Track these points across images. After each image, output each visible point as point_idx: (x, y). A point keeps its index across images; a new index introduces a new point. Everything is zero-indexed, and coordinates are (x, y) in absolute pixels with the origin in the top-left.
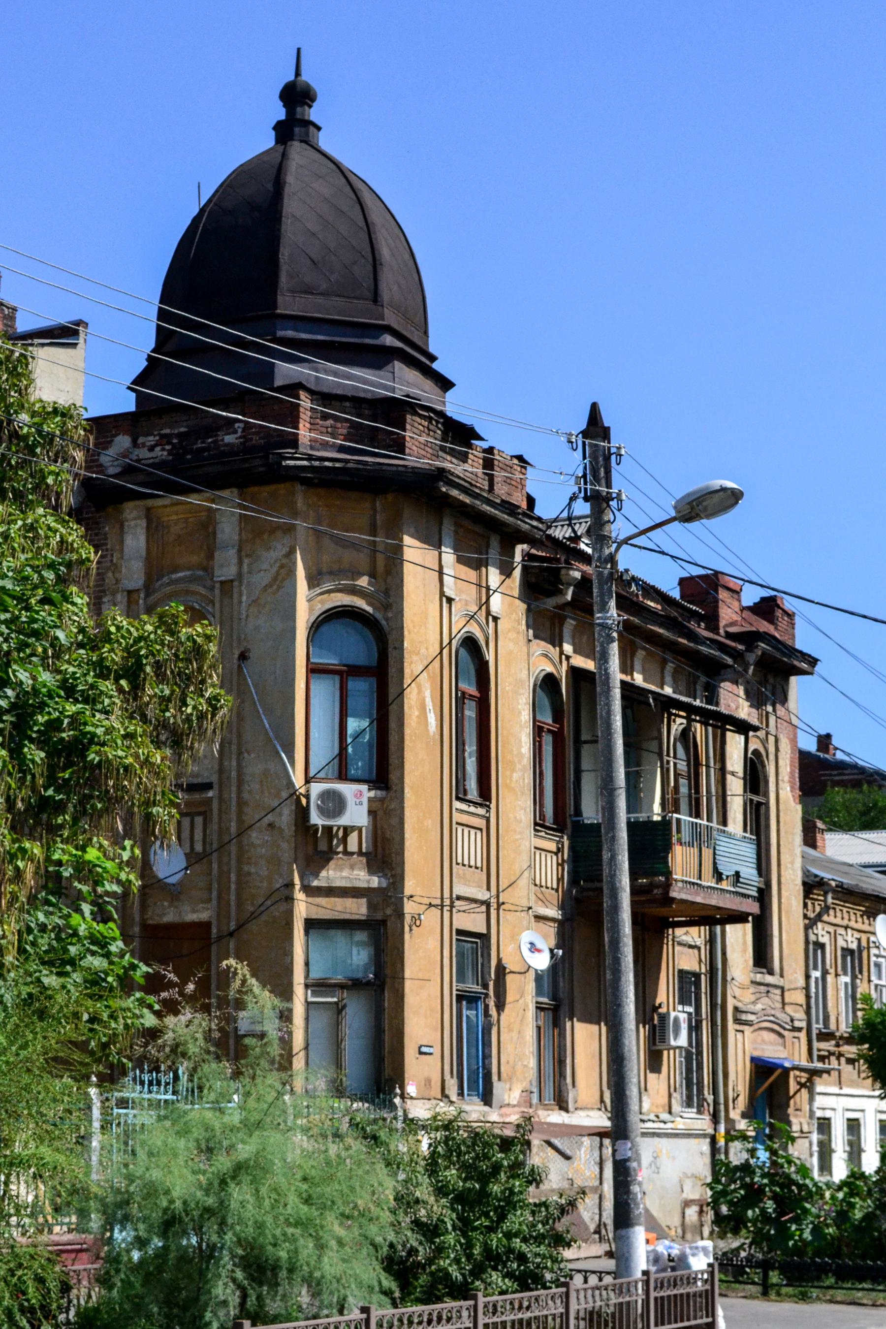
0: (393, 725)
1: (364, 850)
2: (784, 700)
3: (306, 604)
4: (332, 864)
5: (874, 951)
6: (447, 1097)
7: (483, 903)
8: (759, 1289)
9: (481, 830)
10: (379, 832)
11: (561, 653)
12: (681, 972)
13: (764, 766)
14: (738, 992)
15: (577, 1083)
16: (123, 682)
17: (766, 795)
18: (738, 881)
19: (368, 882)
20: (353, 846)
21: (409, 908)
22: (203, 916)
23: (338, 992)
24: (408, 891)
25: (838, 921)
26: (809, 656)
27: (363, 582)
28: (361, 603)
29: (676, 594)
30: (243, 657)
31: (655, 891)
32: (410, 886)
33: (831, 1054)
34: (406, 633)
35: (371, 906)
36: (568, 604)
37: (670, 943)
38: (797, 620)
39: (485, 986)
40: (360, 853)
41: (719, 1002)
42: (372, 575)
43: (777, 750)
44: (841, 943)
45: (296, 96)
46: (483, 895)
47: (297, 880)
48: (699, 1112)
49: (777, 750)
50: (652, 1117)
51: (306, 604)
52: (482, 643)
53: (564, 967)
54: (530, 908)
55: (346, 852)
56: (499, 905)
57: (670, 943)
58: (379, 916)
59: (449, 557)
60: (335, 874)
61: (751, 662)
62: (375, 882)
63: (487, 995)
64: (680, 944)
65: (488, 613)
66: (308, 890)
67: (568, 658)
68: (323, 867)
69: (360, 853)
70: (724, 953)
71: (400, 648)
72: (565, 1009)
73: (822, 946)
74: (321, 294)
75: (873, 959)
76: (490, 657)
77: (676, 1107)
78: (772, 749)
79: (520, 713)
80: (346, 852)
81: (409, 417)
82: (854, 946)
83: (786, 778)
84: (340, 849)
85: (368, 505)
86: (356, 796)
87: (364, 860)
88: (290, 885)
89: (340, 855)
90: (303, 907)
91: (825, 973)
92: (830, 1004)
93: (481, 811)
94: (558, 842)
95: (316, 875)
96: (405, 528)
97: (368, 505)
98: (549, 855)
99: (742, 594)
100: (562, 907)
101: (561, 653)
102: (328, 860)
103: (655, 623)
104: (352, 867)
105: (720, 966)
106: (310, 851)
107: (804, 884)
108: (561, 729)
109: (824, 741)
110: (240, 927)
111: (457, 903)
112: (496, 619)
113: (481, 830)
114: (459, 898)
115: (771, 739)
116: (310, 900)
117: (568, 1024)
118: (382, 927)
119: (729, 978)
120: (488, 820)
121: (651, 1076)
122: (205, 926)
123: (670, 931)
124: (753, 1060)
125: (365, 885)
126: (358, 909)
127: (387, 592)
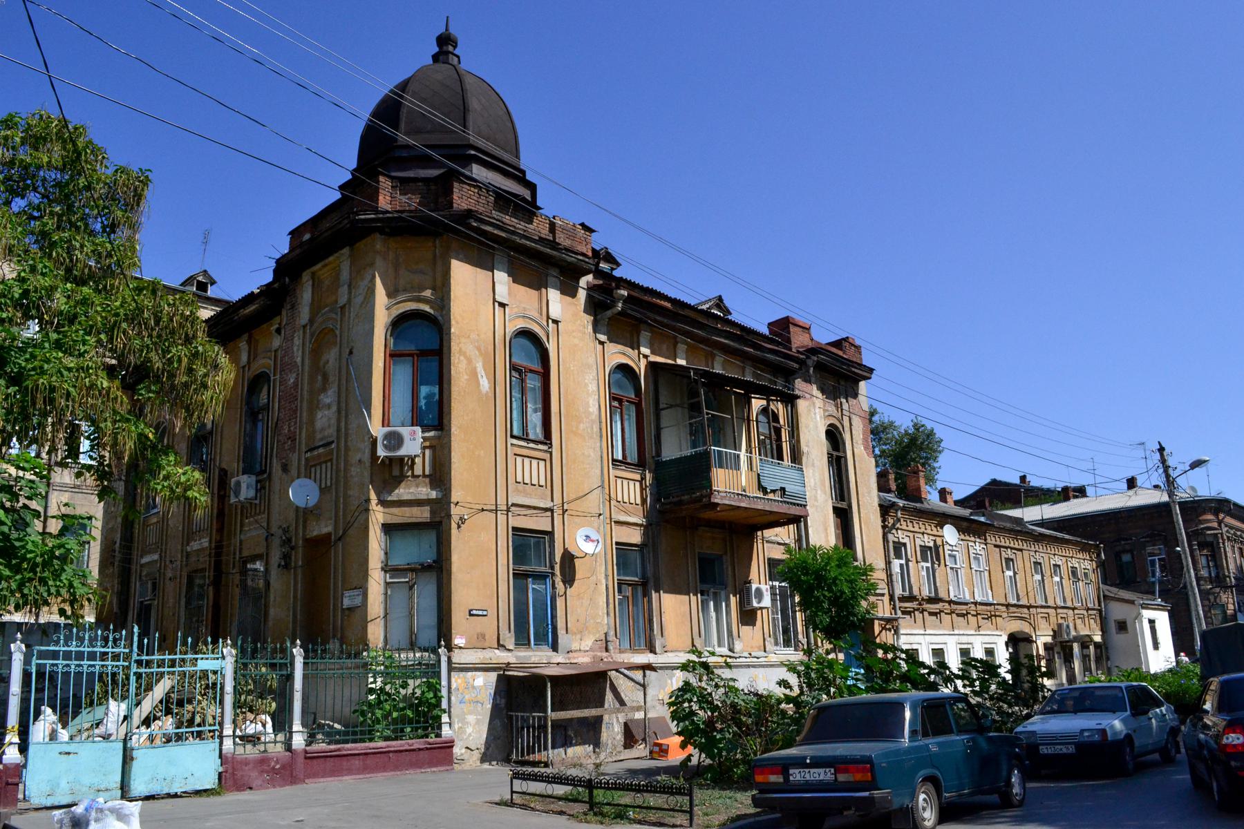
1: (427, 472)
2: (855, 395)
3: (383, 310)
4: (403, 485)
5: (947, 547)
6: (503, 646)
7: (546, 510)
8: (585, 807)
15: (665, 633)
16: (103, 336)
17: (845, 452)
20: (418, 470)
21: (455, 511)
22: (325, 530)
23: (409, 575)
24: (454, 499)
25: (916, 529)
27: (428, 293)
28: (427, 308)
29: (765, 331)
30: (351, 353)
32: (455, 496)
33: (915, 610)
34: (453, 322)
35: (432, 512)
36: (620, 313)
37: (760, 546)
38: (863, 350)
39: (552, 568)
40: (424, 476)
42: (434, 289)
44: (919, 542)
45: (445, 41)
46: (549, 505)
47: (373, 496)
48: (796, 650)
50: (746, 654)
51: (383, 310)
52: (545, 339)
55: (413, 476)
56: (564, 511)
57: (760, 546)
58: (438, 519)
59: (501, 277)
60: (404, 492)
62: (434, 494)
63: (553, 574)
65: (548, 317)
66: (382, 503)
67: (646, 357)
68: (396, 488)
69: (424, 476)
71: (449, 334)
72: (651, 583)
73: (905, 545)
74: (428, 132)
75: (947, 553)
76: (551, 348)
77: (769, 647)
78: (846, 424)
79: (586, 385)
80: (413, 476)
81: (456, 185)
82: (931, 544)
83: (860, 442)
84: (410, 473)
85: (430, 244)
87: (427, 480)
88: (368, 501)
90: (378, 516)
91: (908, 561)
92: (912, 580)
93: (545, 448)
95: (390, 492)
97: (430, 244)
98: (631, 483)
99: (812, 331)
100: (647, 516)
102: (400, 483)
103: (718, 336)
104: (417, 486)
106: (387, 476)
107: (880, 506)
108: (640, 401)
109: (1023, 478)
110: (344, 533)
111: (513, 509)
112: (556, 322)
114: (513, 505)
115: (846, 419)
116: (387, 510)
117: (654, 595)
118: (437, 525)
120: (551, 453)
121: (746, 629)
122: (329, 534)
126: (423, 514)
127: (442, 300)
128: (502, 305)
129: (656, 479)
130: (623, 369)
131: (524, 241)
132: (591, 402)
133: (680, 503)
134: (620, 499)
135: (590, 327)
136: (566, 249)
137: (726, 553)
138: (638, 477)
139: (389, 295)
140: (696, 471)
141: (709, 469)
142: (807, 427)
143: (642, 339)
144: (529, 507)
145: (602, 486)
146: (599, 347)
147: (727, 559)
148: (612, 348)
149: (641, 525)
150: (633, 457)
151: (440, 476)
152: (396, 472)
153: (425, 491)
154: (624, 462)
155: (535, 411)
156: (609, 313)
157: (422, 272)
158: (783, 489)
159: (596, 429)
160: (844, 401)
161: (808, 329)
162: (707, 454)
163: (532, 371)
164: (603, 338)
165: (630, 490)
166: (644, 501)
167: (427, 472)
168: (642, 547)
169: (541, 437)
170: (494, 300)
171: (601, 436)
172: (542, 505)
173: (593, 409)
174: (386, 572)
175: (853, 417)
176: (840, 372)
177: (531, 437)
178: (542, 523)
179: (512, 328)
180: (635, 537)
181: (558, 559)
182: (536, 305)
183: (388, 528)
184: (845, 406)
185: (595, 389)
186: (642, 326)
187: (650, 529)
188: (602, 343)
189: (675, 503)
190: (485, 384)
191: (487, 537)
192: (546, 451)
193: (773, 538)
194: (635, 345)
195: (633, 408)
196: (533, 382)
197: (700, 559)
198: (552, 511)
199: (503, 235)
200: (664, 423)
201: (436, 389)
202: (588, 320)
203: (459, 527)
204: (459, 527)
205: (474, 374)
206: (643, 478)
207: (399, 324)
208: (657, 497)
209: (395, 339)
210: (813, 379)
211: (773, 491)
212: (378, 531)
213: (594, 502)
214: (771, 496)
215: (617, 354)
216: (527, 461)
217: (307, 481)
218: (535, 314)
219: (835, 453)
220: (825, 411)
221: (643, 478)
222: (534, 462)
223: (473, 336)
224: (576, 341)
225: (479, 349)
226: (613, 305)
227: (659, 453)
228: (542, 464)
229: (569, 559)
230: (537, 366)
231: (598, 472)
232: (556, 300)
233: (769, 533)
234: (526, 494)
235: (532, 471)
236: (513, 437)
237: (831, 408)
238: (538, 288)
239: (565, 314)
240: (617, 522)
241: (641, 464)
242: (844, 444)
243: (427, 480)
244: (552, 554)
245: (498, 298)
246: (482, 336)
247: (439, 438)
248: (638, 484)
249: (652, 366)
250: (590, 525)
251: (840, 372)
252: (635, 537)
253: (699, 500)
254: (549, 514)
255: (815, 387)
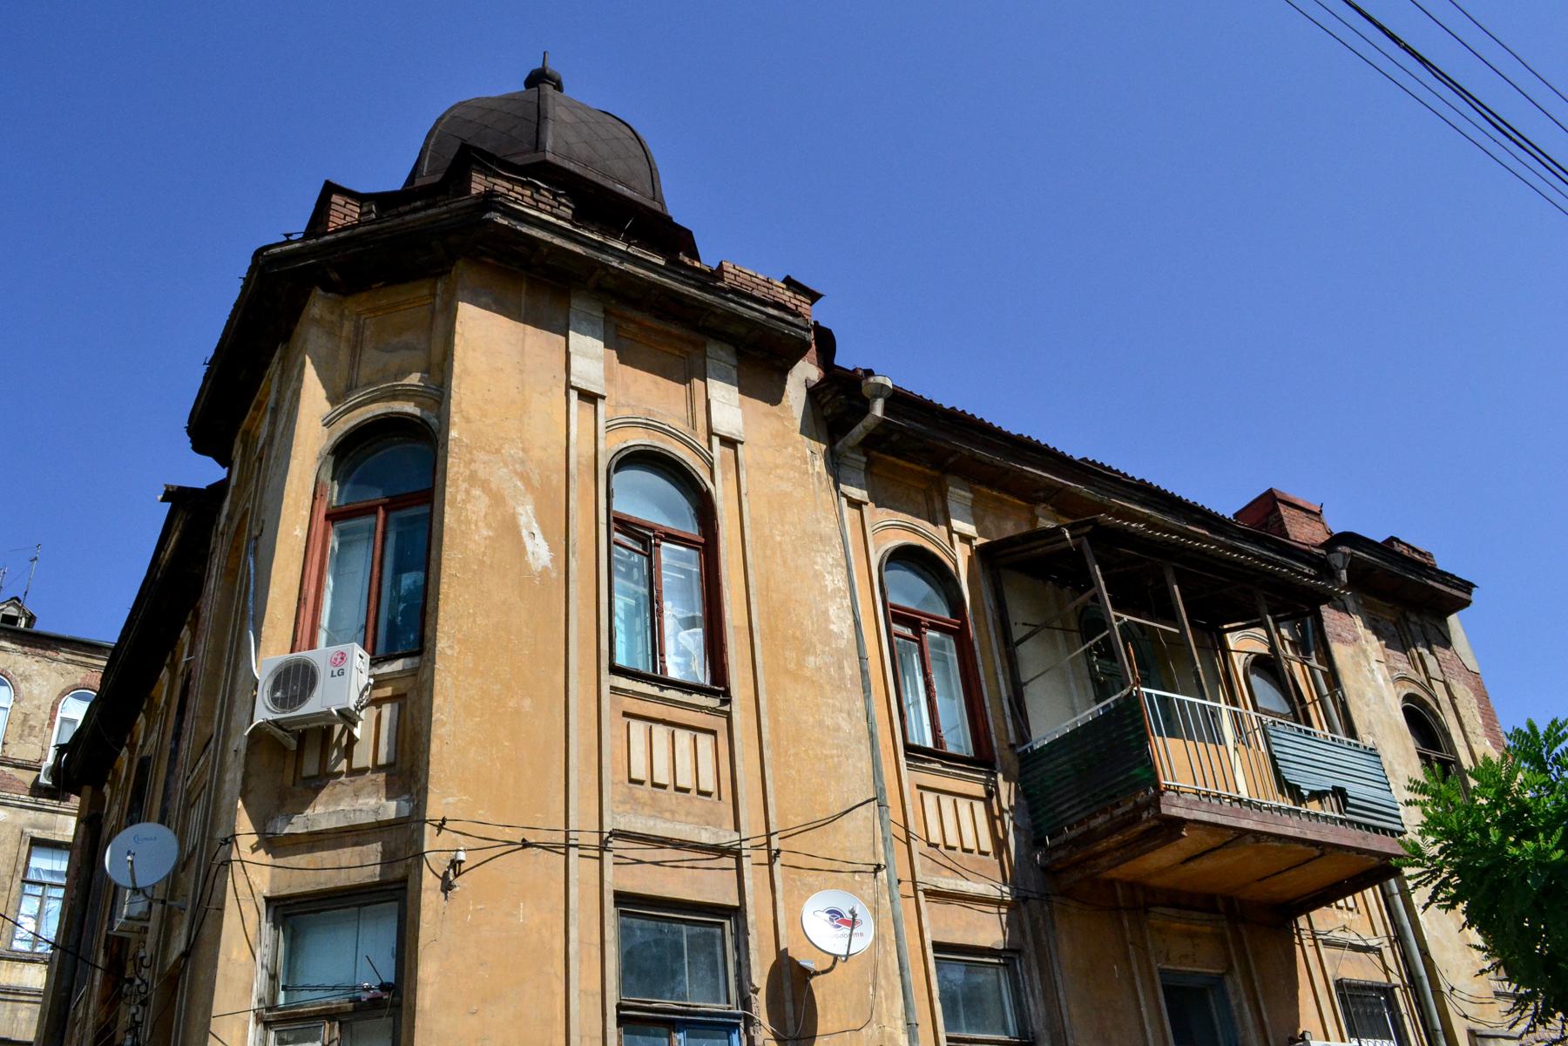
0: (433, 552)
2: (1446, 643)
4: (323, 795)
7: (719, 851)
9: (714, 733)
10: (409, 726)
11: (951, 531)
12: (1339, 984)
13: (1437, 718)
14: (1470, 1010)
17: (1452, 749)
18: (1346, 804)
19: (376, 812)
24: (434, 810)
26: (1453, 576)
28: (409, 408)
31: (1145, 815)
34: (455, 418)
35: (388, 860)
37: (1311, 952)
39: (746, 1003)
40: (377, 768)
41: (1439, 1026)
43: (1452, 697)
46: (727, 837)
47: (244, 823)
49: (1452, 697)
52: (704, 474)
53: (1031, 979)
54: (878, 868)
56: (773, 857)
57: (1311, 952)
58: (398, 872)
60: (323, 813)
61: (1340, 564)
62: (390, 810)
63: (749, 1021)
64: (1327, 943)
65: (710, 433)
66: (272, 843)
70: (1425, 954)
76: (722, 493)
79: (818, 576)
83: (1480, 731)
86: (334, 663)
87: (381, 777)
89: (343, 778)
90: (254, 875)
93: (713, 702)
94: (986, 785)
96: (459, 293)
97: (425, 291)
98: (963, 805)
99: (1325, 516)
100: (1015, 879)
101: (951, 531)
102: (317, 791)
104: (356, 795)
105: (1423, 972)
108: (964, 623)
111: (615, 843)
112: (730, 442)
113: (714, 733)
116: (280, 862)
119: (1445, 989)
123: (1302, 922)
124: (268, 900)
125: (371, 819)
126: (359, 865)
128: (589, 397)
129: (1025, 794)
130: (907, 557)
131: (627, 267)
132: (833, 611)
133: (1090, 837)
134: (935, 837)
135: (820, 465)
136: (734, 291)
137: (1230, 968)
138: (979, 790)
139: (333, 399)
140: (1113, 755)
141: (1143, 739)
142: (1361, 696)
143: (952, 506)
144: (679, 844)
145: (879, 800)
146: (850, 514)
147: (1235, 985)
148: (878, 516)
149: (999, 903)
150: (958, 740)
151: (406, 770)
152: (310, 767)
153: (372, 804)
154: (937, 754)
155: (690, 623)
156: (858, 432)
157: (409, 347)
158: (1339, 793)
159: (851, 669)
160: (1425, 652)
161: (1318, 514)
162: (1133, 703)
163: (671, 538)
164: (859, 494)
165: (962, 821)
166: (1000, 845)
167: (382, 760)
168: (1008, 956)
169: (702, 677)
170: (569, 386)
171: (866, 690)
172: (706, 838)
173: (841, 625)
174: (267, 1025)
175: (1453, 683)
176: (1411, 597)
177: (673, 673)
178: (712, 886)
179: (612, 444)
180: (989, 931)
181: (759, 976)
182: (681, 409)
183: (288, 912)
184: (1431, 662)
185: (842, 584)
186: (949, 479)
187: (1017, 909)
188: (856, 504)
189: (1075, 842)
190: (540, 552)
191: (535, 917)
192: (713, 711)
193: (1338, 935)
194: (939, 516)
195: (950, 642)
196: (676, 564)
197: (1166, 989)
198: (738, 855)
199: (578, 249)
200: (1026, 673)
201: (421, 575)
202: (812, 454)
203: (447, 887)
204: (447, 887)
205: (510, 530)
206: (991, 795)
207: (349, 453)
208: (1033, 837)
209: (341, 485)
210: (1351, 605)
211: (1318, 796)
212: (251, 917)
213: (858, 836)
214: (1314, 807)
215: (893, 528)
216: (660, 732)
217: (163, 828)
218: (680, 426)
219: (1433, 755)
220: (1391, 669)
221: (991, 795)
222: (683, 737)
223: (511, 450)
224: (786, 487)
225: (525, 477)
226: (866, 408)
227: (1023, 733)
228: (705, 741)
229: (793, 983)
230: (691, 530)
231: (866, 766)
232: (727, 405)
233: (1326, 919)
234: (659, 813)
235: (688, 758)
236: (615, 670)
237: (1402, 663)
238: (685, 380)
239: (760, 442)
240: (935, 894)
241: (981, 760)
242: (1448, 736)
243: (381, 777)
244: (743, 966)
245: (574, 380)
246: (537, 453)
247: (413, 673)
248: (979, 807)
249: (984, 557)
250: (853, 890)
251: (1411, 597)
252: (989, 931)
253: (1133, 819)
254: (730, 862)
255: (1358, 621)
